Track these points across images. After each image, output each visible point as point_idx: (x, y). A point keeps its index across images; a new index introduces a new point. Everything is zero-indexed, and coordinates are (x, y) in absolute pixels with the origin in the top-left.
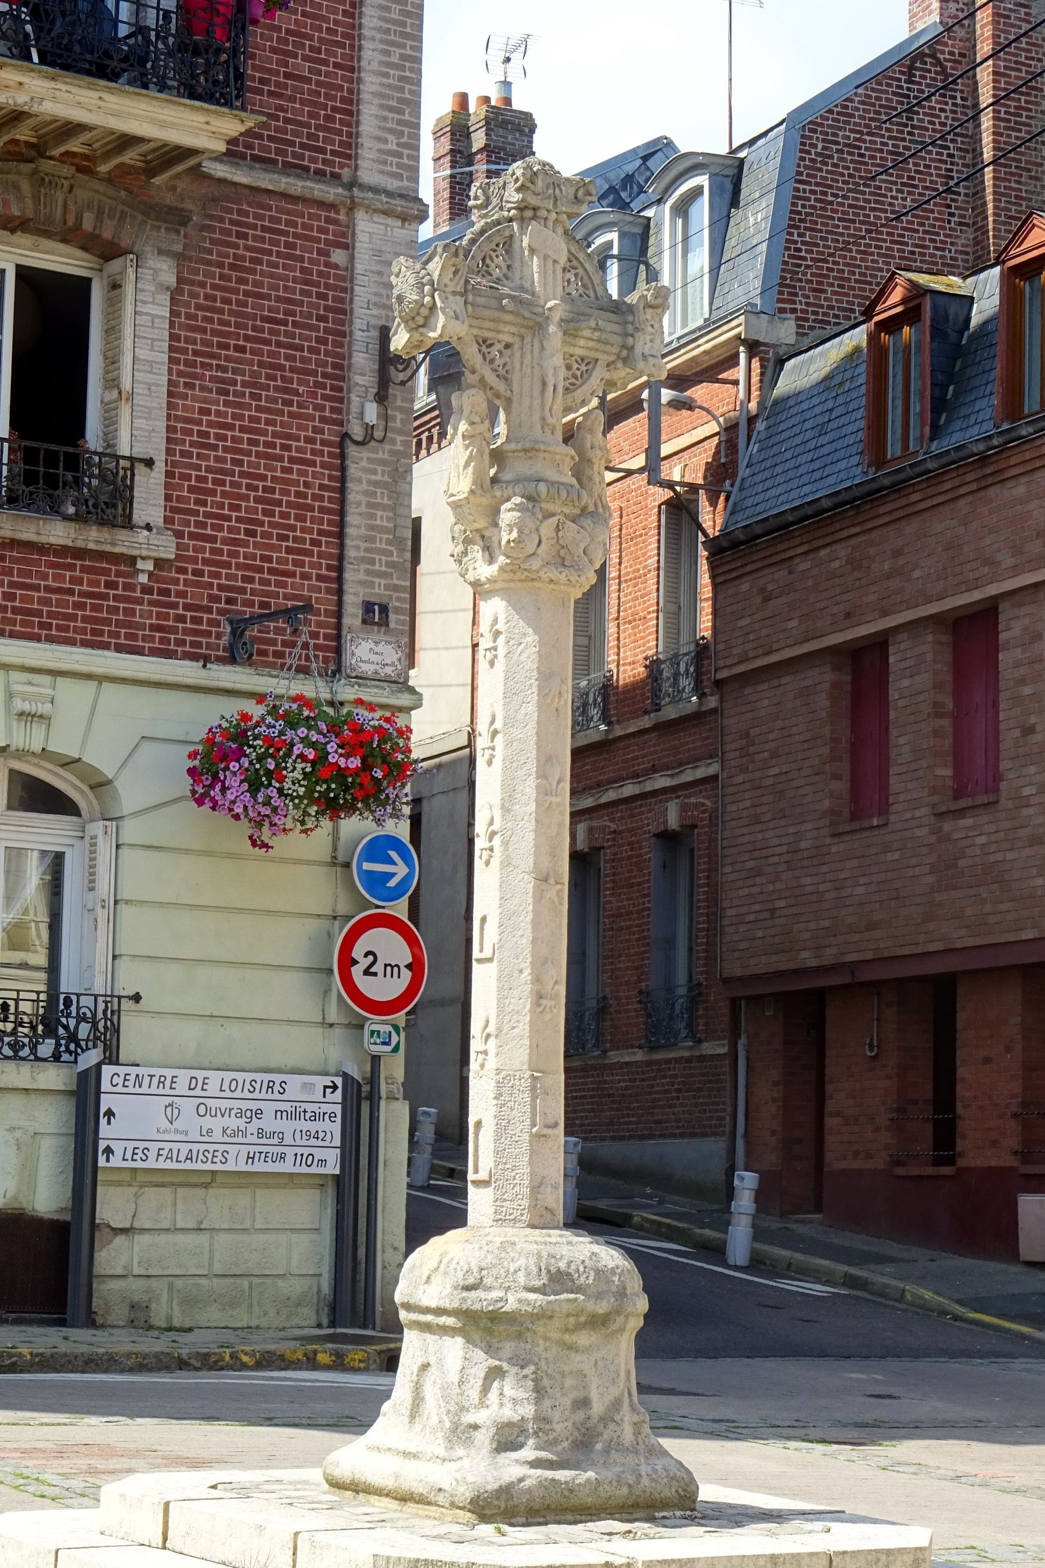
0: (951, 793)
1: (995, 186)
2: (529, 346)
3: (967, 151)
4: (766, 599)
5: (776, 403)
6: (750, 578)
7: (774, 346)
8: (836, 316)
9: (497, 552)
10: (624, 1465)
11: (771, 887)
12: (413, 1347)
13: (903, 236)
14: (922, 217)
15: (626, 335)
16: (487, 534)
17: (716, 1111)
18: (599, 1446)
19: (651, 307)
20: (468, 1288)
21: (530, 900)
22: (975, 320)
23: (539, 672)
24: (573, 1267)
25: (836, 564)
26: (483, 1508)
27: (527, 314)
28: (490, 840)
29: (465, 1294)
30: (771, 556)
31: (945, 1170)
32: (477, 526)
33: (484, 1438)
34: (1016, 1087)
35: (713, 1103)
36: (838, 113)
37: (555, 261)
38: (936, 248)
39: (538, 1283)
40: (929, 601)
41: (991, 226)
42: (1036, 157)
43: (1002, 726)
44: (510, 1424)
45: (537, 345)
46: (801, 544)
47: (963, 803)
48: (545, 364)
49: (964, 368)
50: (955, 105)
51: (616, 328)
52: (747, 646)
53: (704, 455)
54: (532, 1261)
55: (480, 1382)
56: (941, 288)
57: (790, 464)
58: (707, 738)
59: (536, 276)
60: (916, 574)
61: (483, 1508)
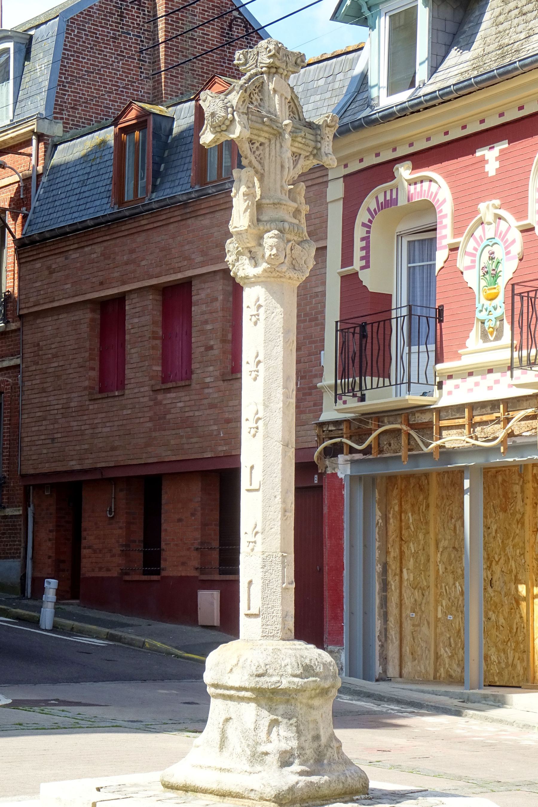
0: (160, 379)
1: (165, 59)
2: (274, 145)
3: (150, 39)
4: (51, 273)
5: (53, 168)
6: (41, 261)
7: (52, 137)
8: (83, 123)
9: (260, 261)
10: (338, 771)
11: (52, 427)
12: (217, 709)
13: (117, 82)
14: (127, 73)
15: (317, 141)
16: (253, 250)
17: (14, 545)
18: (325, 762)
19: (329, 126)
20: (259, 676)
21: (280, 457)
22: (176, 130)
23: (284, 329)
24: (313, 662)
25: (94, 256)
26: (281, 800)
27: (275, 128)
28: (256, 423)
29: (257, 679)
30: (55, 249)
31: (155, 578)
32: (249, 245)
33: (273, 760)
34: (198, 535)
35: (12, 541)
36: (86, 14)
37: (286, 98)
38: (134, 90)
39: (298, 672)
40: (151, 277)
41: (163, 80)
42: (186, 45)
43: (193, 346)
44: (285, 752)
45: (278, 145)
46: (74, 244)
47: (170, 385)
48: (283, 156)
49: (170, 155)
50: (144, 14)
51: (312, 137)
52: (39, 297)
53: (10, 192)
54: (293, 660)
55: (267, 728)
56: (158, 112)
57: (64, 201)
58: (10, 345)
59: (277, 106)
60: (143, 263)
61: (281, 800)
